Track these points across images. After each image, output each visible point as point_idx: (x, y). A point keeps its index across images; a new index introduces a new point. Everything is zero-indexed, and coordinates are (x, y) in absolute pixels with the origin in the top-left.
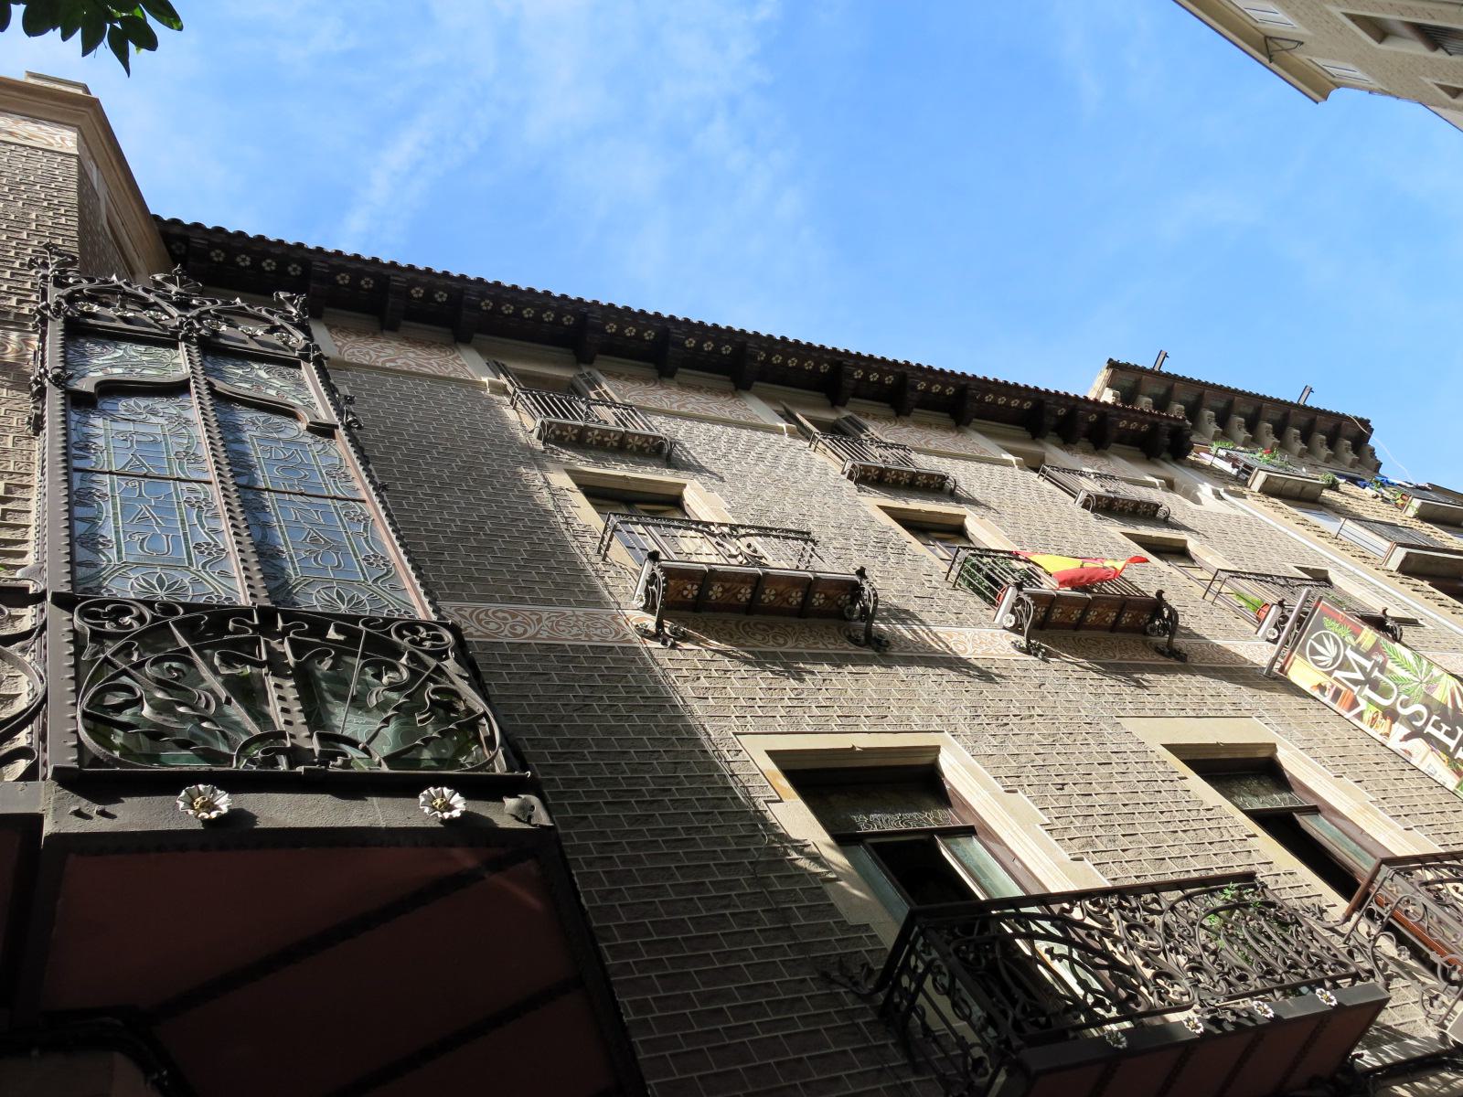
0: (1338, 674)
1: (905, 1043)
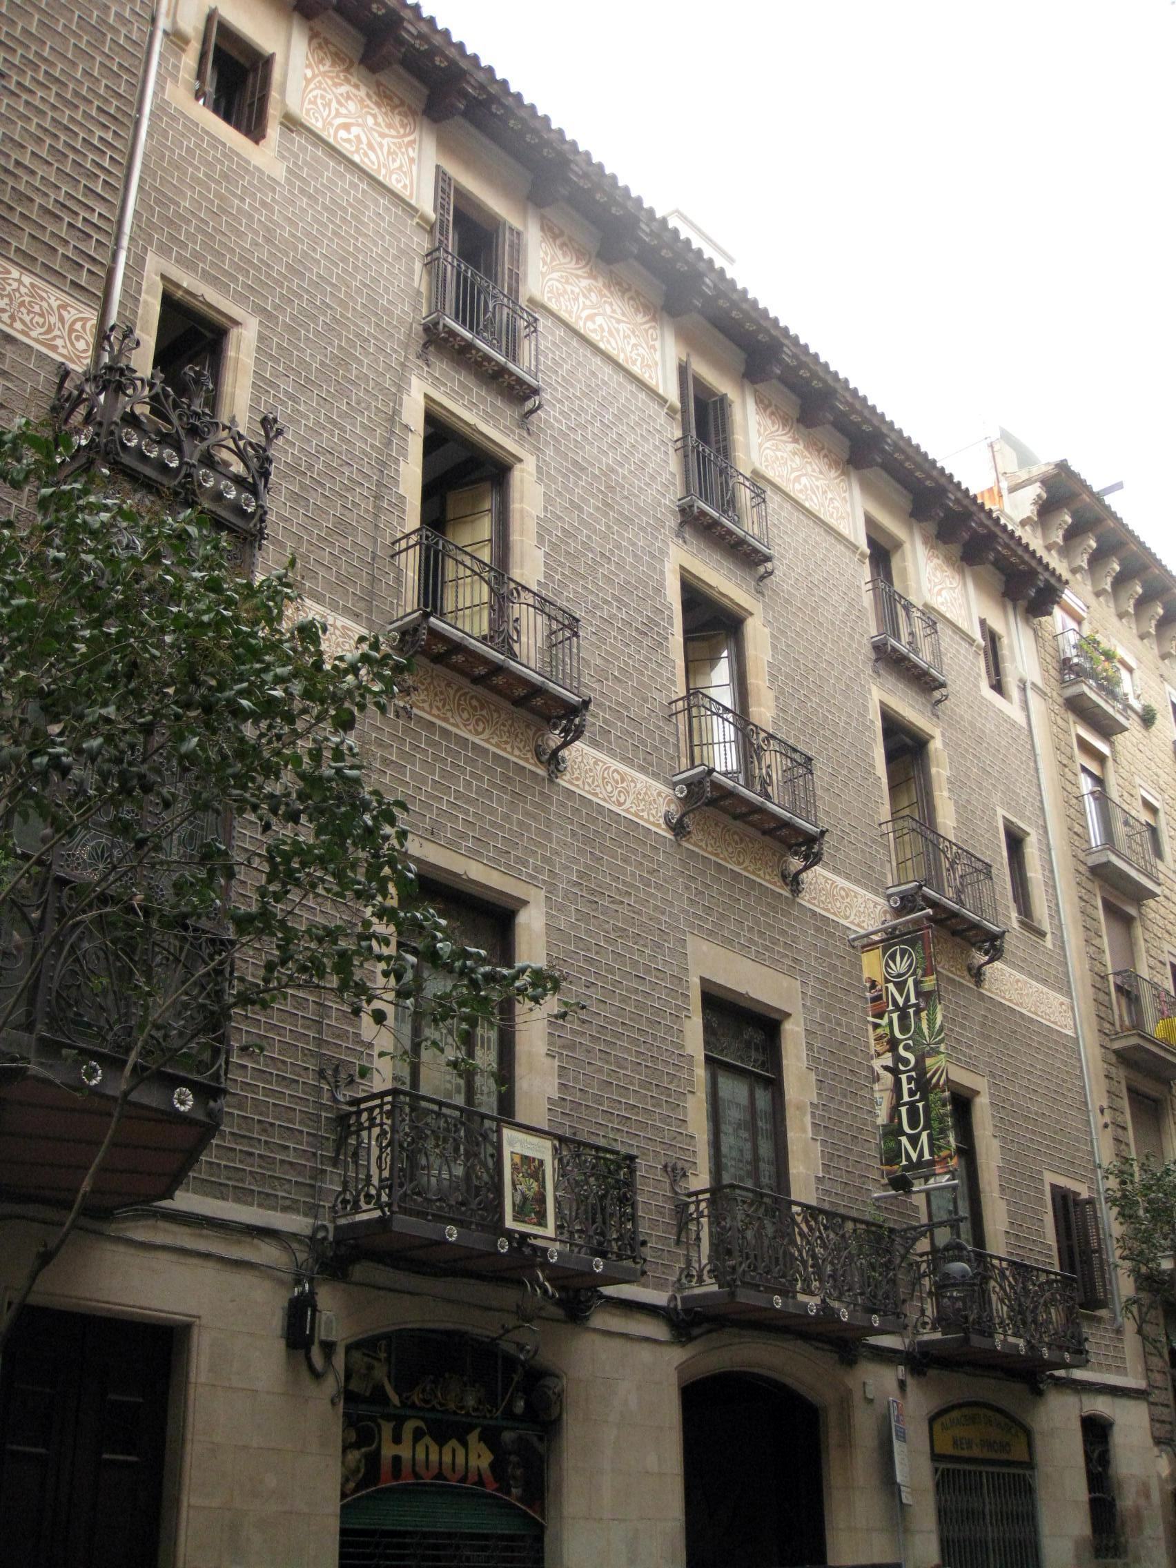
0: (891, 986)
1: (341, 1143)
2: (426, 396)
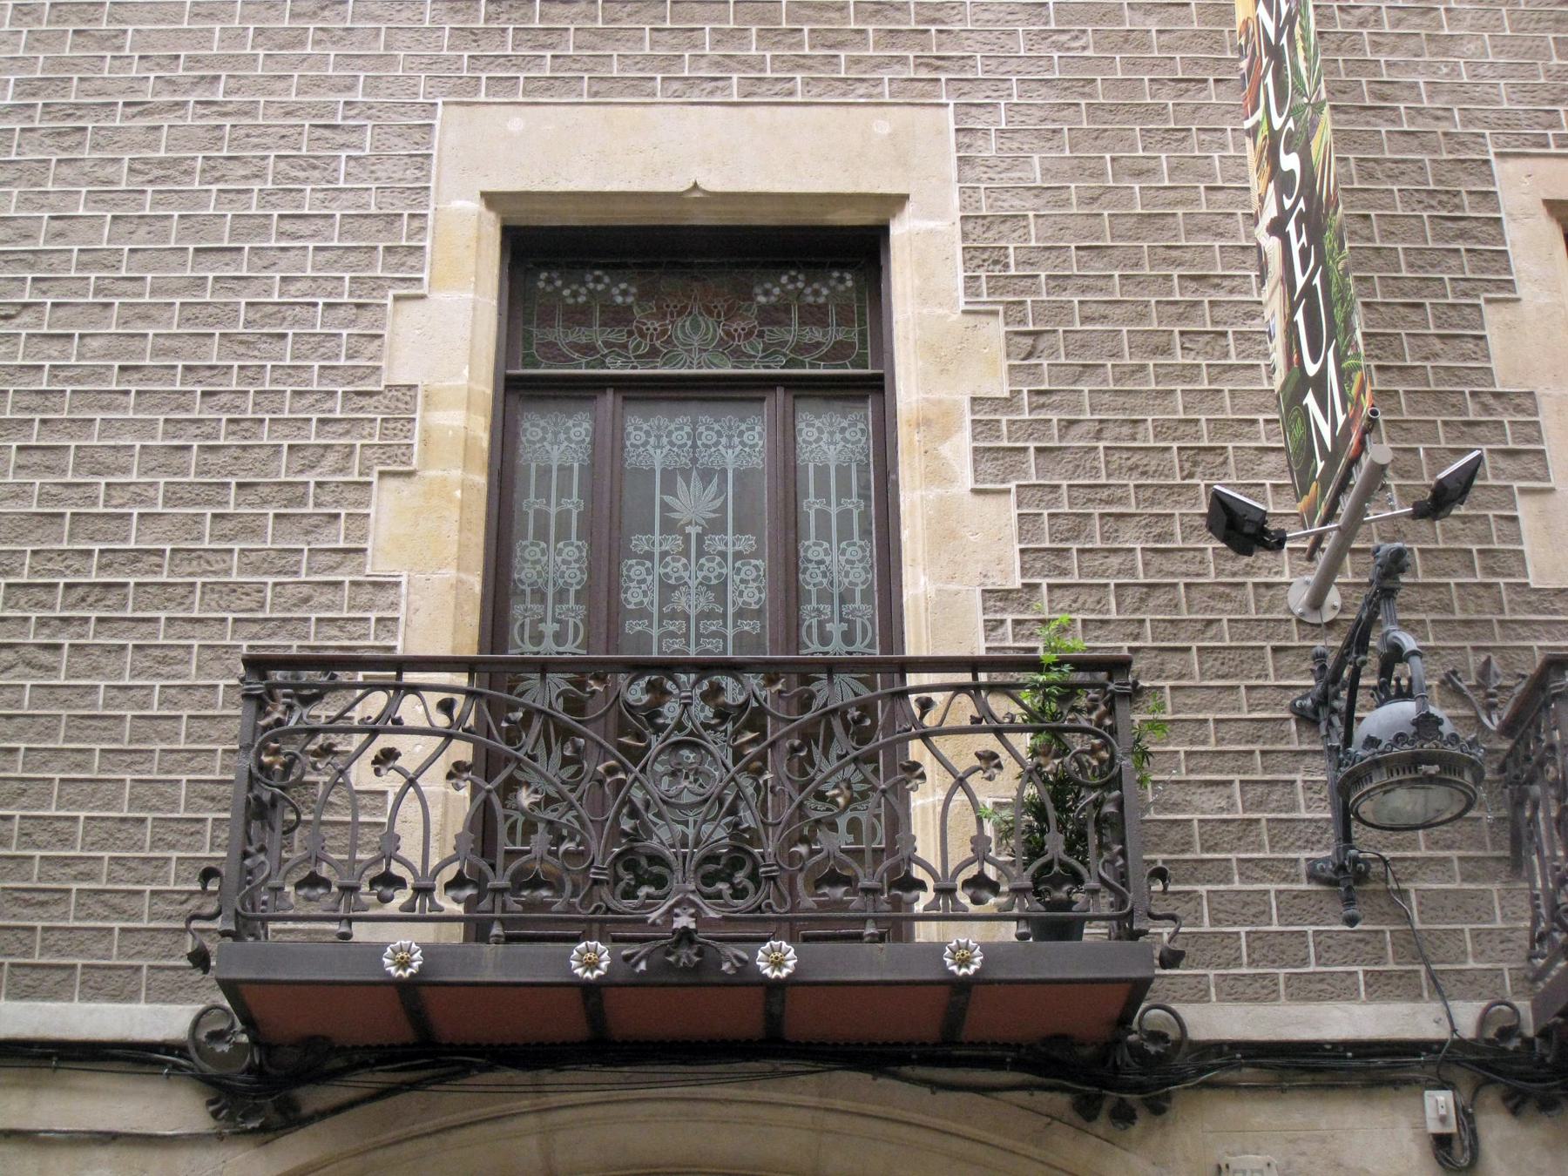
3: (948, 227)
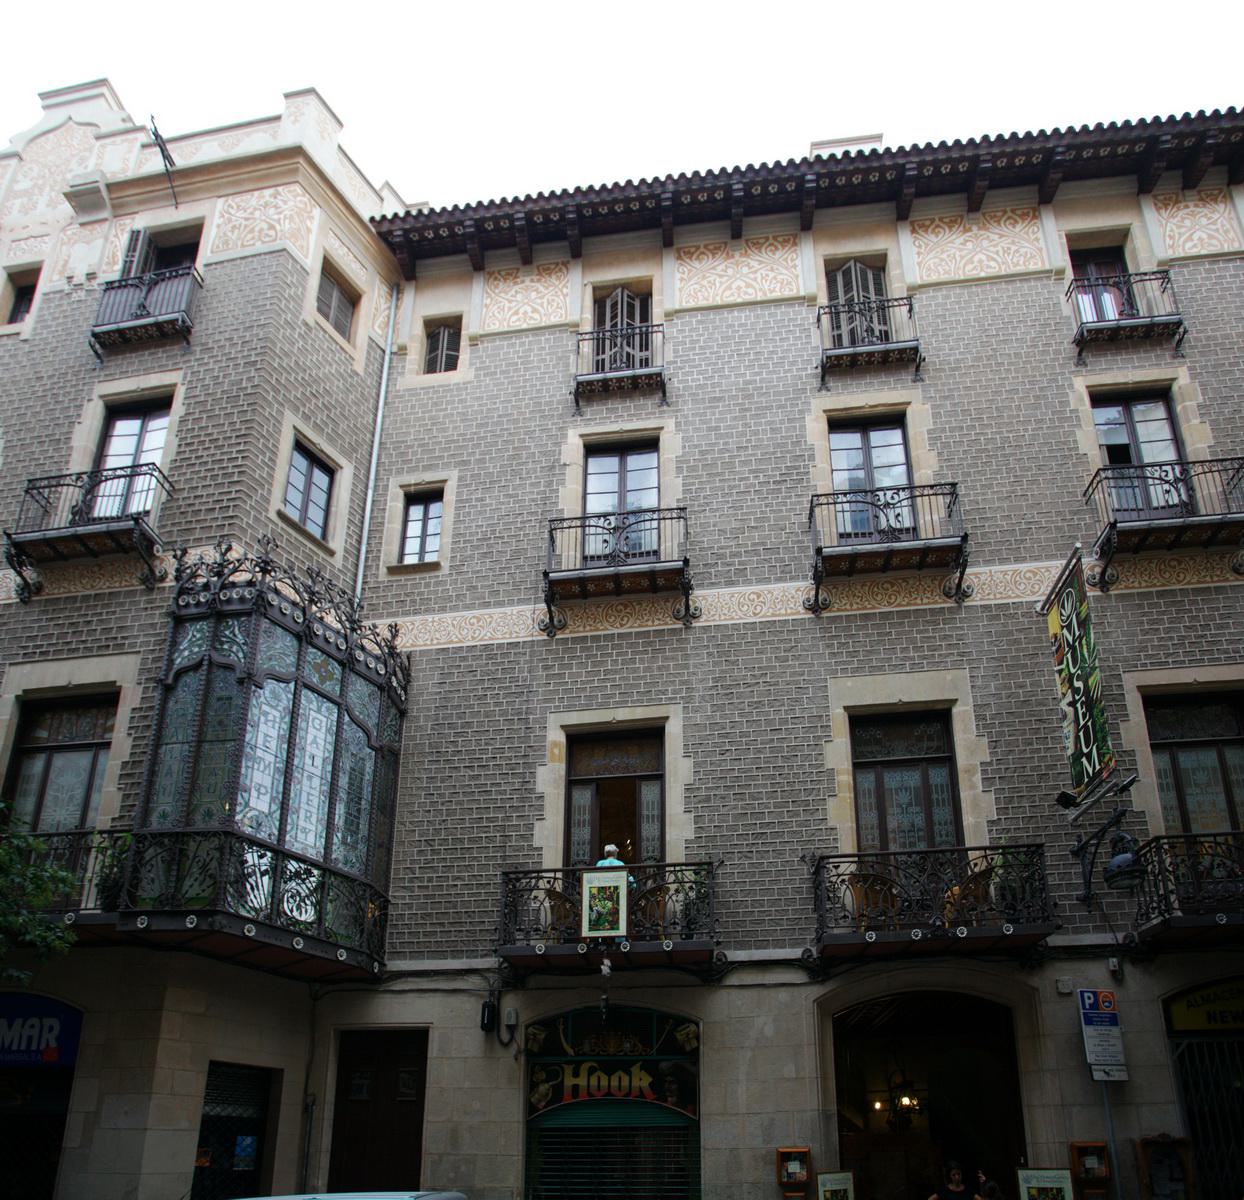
2: (581, 436)
3: (970, 708)
